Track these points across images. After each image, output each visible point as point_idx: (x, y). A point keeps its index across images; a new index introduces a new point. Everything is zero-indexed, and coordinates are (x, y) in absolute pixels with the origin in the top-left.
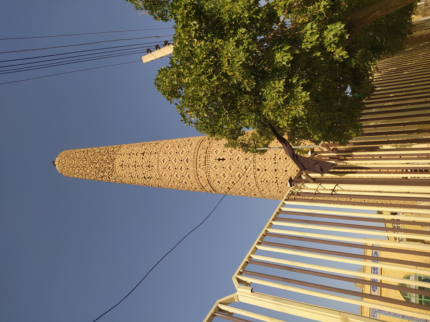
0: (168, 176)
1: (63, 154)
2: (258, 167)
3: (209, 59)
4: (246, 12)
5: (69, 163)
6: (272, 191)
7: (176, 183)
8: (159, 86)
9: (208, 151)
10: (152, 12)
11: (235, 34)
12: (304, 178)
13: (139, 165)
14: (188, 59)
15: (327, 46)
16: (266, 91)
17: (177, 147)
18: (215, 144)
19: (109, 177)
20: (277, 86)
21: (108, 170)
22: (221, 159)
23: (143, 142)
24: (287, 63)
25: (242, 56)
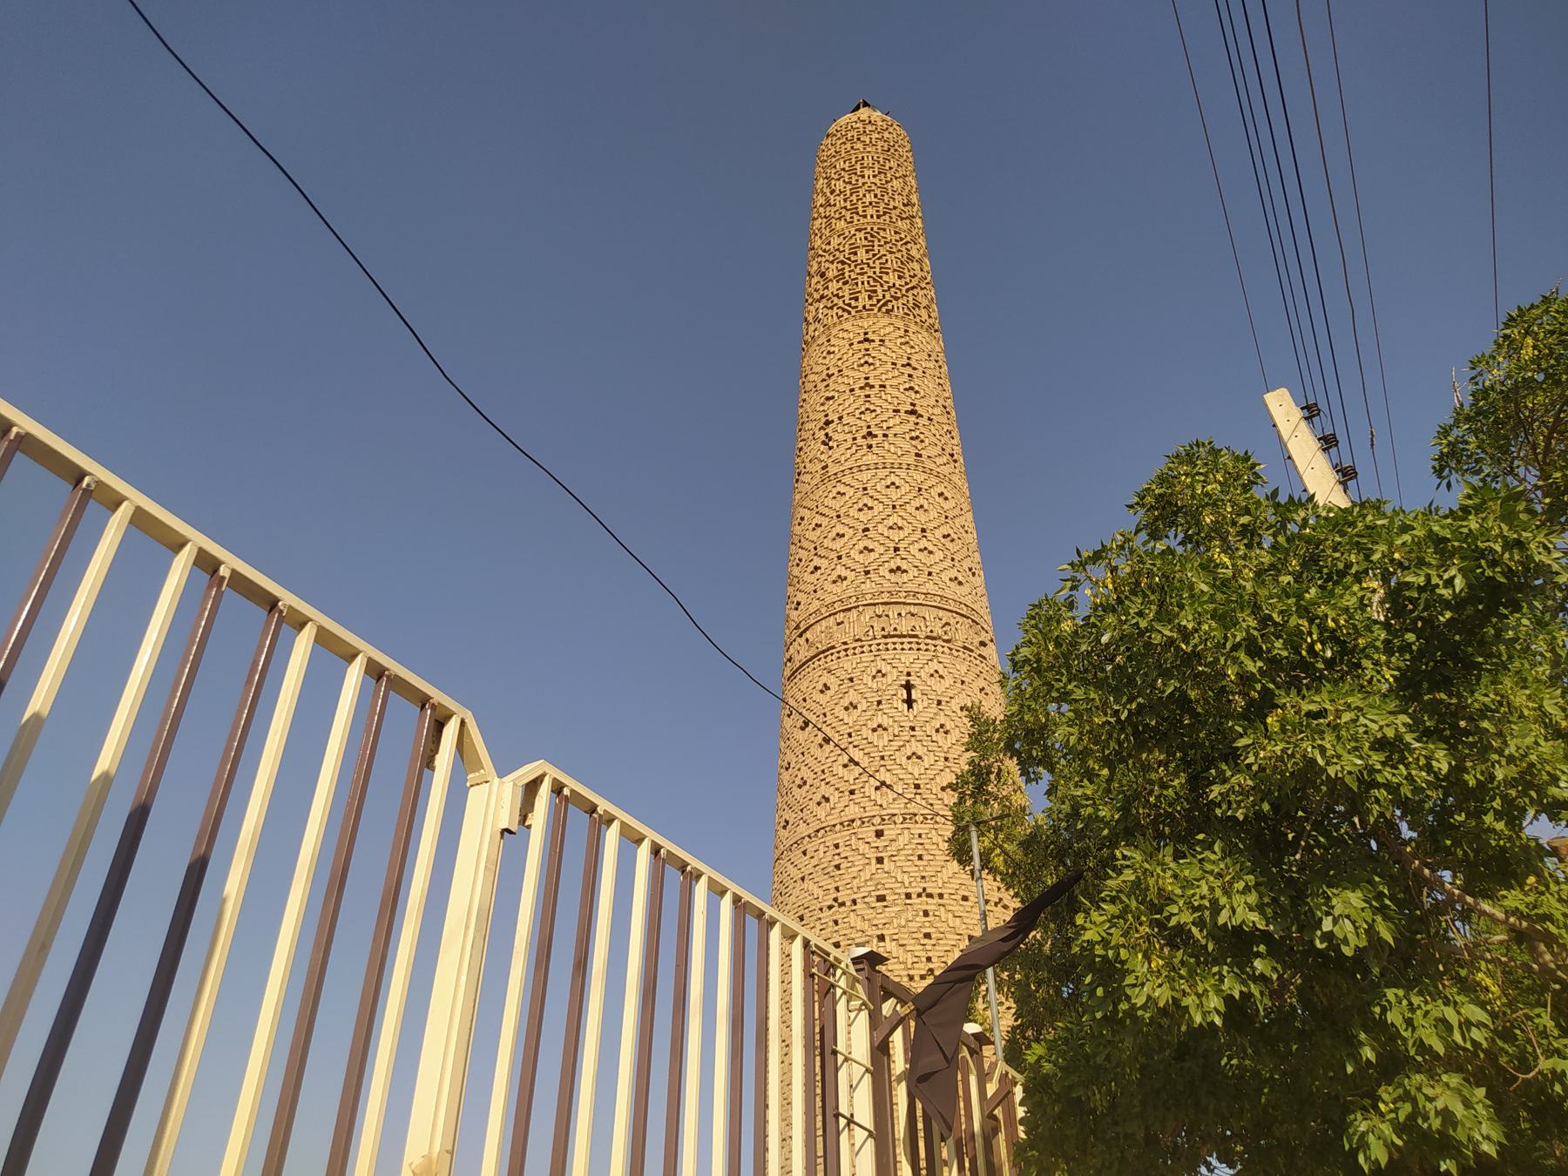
0: (836, 504)
1: (897, 133)
2: (889, 832)
3: (1319, 640)
4: (1513, 771)
5: (867, 157)
6: (805, 885)
7: (812, 535)
8: (1190, 458)
9: (939, 642)
10: (1468, 419)
11: (1426, 735)
12: (887, 1007)
13: (873, 399)
14: (1311, 562)
15: (1401, 1085)
16: (1213, 857)
17: (945, 530)
18: (964, 669)
19: (822, 297)
20: (1238, 900)
21: (846, 294)
22: (909, 694)
23: (956, 408)
24: (1329, 936)
25: (1347, 765)
